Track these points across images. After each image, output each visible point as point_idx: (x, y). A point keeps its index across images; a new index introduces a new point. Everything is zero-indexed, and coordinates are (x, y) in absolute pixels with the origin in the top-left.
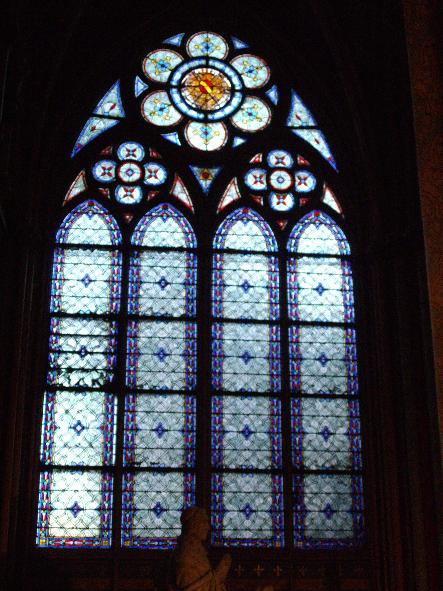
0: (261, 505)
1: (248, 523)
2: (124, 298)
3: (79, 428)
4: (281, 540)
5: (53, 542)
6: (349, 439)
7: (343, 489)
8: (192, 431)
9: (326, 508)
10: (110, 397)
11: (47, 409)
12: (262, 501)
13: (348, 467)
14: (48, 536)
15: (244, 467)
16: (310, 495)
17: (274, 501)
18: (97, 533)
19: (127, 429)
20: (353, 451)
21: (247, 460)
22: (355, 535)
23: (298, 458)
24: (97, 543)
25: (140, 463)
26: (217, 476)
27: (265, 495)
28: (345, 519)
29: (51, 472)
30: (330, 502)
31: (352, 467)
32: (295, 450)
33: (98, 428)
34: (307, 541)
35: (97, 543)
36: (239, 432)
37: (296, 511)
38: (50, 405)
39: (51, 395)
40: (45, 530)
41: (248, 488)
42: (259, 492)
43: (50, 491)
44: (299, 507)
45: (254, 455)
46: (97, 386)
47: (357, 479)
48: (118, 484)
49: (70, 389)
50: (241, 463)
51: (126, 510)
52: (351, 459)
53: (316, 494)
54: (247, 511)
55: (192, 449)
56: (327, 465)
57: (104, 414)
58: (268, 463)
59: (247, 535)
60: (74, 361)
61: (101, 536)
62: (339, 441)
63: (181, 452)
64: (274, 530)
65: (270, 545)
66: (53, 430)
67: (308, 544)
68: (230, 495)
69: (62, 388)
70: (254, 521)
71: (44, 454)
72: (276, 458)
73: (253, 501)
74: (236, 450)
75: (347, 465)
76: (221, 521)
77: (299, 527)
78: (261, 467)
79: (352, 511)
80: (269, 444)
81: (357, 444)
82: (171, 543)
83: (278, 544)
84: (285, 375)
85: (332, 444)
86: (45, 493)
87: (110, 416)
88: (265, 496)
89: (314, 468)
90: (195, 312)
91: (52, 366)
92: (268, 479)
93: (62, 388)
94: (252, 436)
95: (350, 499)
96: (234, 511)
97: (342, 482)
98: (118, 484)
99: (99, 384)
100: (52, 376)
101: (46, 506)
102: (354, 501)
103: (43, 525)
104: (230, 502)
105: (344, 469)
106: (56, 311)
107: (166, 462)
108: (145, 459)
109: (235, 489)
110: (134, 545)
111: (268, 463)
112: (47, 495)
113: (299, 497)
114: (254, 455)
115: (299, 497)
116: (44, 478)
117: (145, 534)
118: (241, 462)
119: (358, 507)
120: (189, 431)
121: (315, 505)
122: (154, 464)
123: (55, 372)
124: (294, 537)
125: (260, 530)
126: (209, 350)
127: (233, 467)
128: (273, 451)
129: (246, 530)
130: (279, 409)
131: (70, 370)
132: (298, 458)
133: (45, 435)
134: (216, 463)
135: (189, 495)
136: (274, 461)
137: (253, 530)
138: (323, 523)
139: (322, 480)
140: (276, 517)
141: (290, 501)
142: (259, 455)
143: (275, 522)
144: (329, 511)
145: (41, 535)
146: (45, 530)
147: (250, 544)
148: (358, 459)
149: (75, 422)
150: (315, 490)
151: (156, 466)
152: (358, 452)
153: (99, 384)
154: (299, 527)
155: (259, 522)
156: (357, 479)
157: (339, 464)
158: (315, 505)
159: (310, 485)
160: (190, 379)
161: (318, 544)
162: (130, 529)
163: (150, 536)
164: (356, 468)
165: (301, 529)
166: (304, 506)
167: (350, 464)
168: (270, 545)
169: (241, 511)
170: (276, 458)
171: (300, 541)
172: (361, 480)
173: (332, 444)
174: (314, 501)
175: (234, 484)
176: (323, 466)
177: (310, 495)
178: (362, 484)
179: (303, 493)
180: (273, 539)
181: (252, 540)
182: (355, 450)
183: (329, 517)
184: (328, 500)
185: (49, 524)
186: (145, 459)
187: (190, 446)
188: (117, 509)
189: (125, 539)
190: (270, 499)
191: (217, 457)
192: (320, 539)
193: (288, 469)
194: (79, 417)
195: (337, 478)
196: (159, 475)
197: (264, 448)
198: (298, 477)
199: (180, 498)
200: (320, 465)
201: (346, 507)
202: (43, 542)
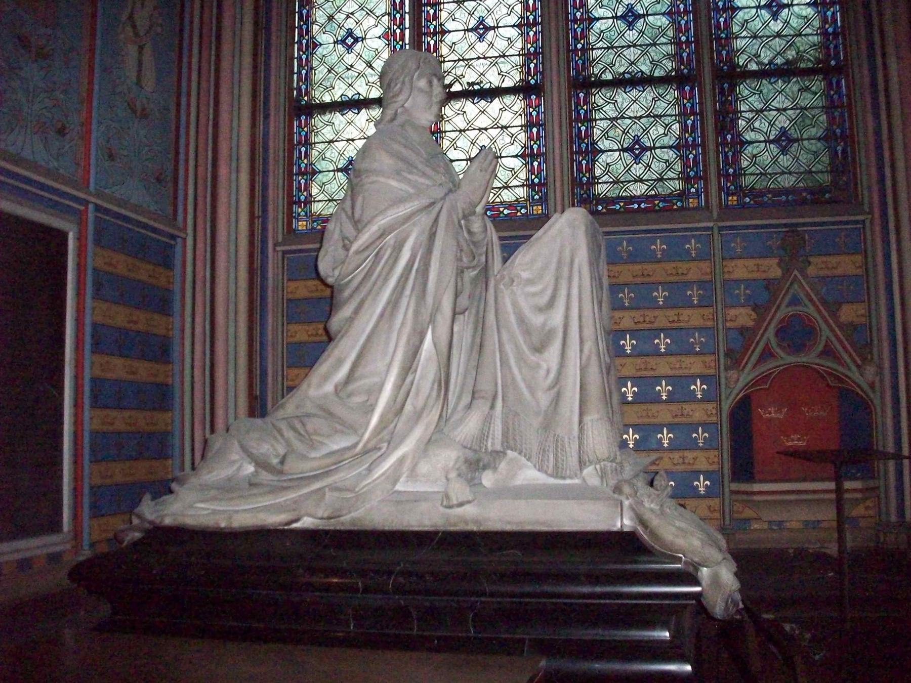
0: (659, 137)
1: (638, 170)
3: (350, 41)
4: (698, 194)
5: (318, 225)
6: (819, 12)
7: (806, 100)
8: (535, 24)
11: (301, 18)
12: (661, 130)
13: (818, 61)
14: (309, 215)
15: (627, 76)
16: (749, 115)
17: (684, 128)
19: (427, 34)
20: (825, 34)
21: (632, 63)
23: (724, 53)
24: (523, 211)
27: (668, 120)
28: (815, 153)
29: (310, 115)
31: (826, 61)
33: (379, 37)
36: (615, 17)
40: (305, 206)
41: (636, 110)
42: (655, 116)
43: (311, 144)
44: (729, 137)
45: (644, 53)
47: (834, 81)
50: (622, 70)
52: (824, 46)
53: (759, 112)
54: (636, 149)
55: (536, 54)
56: (779, 61)
57: (389, 14)
58: (669, 65)
59: (638, 189)
62: (799, 16)
63: (517, 60)
64: (686, 179)
66: (310, 50)
67: (747, 200)
68: (604, 124)
70: (648, 166)
71: (299, 89)
72: (685, 55)
73: (646, 131)
74: (612, 47)
75: (816, 58)
76: (591, 170)
77: (731, 171)
78: (658, 73)
80: (670, 33)
81: (834, 20)
82: (506, 212)
83: (692, 203)
85: (787, 23)
86: (303, 149)
87: (398, 16)
88: (666, 122)
89: (753, 67)
92: (672, 94)
94: (640, 23)
95: (824, 118)
96: (750, 7)
97: (807, 89)
101: (306, 168)
102: (831, 120)
103: (303, 198)
104: (605, 135)
105: (810, 65)
107: (493, 79)
108: (457, 79)
109: (613, 114)
111: (669, 65)
112: (306, 152)
114: (644, 53)
116: (300, 126)
118: (621, 67)
120: (529, 25)
121: (759, 131)
122: (473, 84)
125: (661, 179)
127: (608, 76)
128: (677, 43)
129: (636, 181)
132: (724, 53)
133: (300, 59)
134: (578, 73)
135: (535, 130)
137: (647, 181)
138: (775, 160)
139: (771, 87)
140: (687, 157)
141: (712, 128)
142: (654, 53)
143: (685, 165)
144: (784, 141)
145: (299, 215)
146: (305, 206)
148: (836, 47)
149: (343, 33)
150: (759, 106)
151: (476, 87)
152: (835, 34)
154: (731, 171)
155: (657, 166)
157: (800, 57)
158: (759, 131)
159: (749, 98)
164: (532, 82)
166: (740, 135)
168: (679, 204)
169: (624, 150)
170: (685, 55)
171: (733, 194)
173: (787, 23)
174: (757, 124)
175: (612, 106)
176: (771, 62)
177: (749, 115)
179: (737, 112)
180: (683, 195)
181: (646, 198)
182: (830, 30)
183: (784, 151)
184: (783, 122)
185: (311, 195)
186: (457, 79)
190: (676, 127)
192: (769, 191)
194: (350, 24)
195: (797, 81)
196: (483, 103)
197: (663, 40)
198: (726, 85)
199: (594, 38)
200: (766, 61)
202: (302, 225)
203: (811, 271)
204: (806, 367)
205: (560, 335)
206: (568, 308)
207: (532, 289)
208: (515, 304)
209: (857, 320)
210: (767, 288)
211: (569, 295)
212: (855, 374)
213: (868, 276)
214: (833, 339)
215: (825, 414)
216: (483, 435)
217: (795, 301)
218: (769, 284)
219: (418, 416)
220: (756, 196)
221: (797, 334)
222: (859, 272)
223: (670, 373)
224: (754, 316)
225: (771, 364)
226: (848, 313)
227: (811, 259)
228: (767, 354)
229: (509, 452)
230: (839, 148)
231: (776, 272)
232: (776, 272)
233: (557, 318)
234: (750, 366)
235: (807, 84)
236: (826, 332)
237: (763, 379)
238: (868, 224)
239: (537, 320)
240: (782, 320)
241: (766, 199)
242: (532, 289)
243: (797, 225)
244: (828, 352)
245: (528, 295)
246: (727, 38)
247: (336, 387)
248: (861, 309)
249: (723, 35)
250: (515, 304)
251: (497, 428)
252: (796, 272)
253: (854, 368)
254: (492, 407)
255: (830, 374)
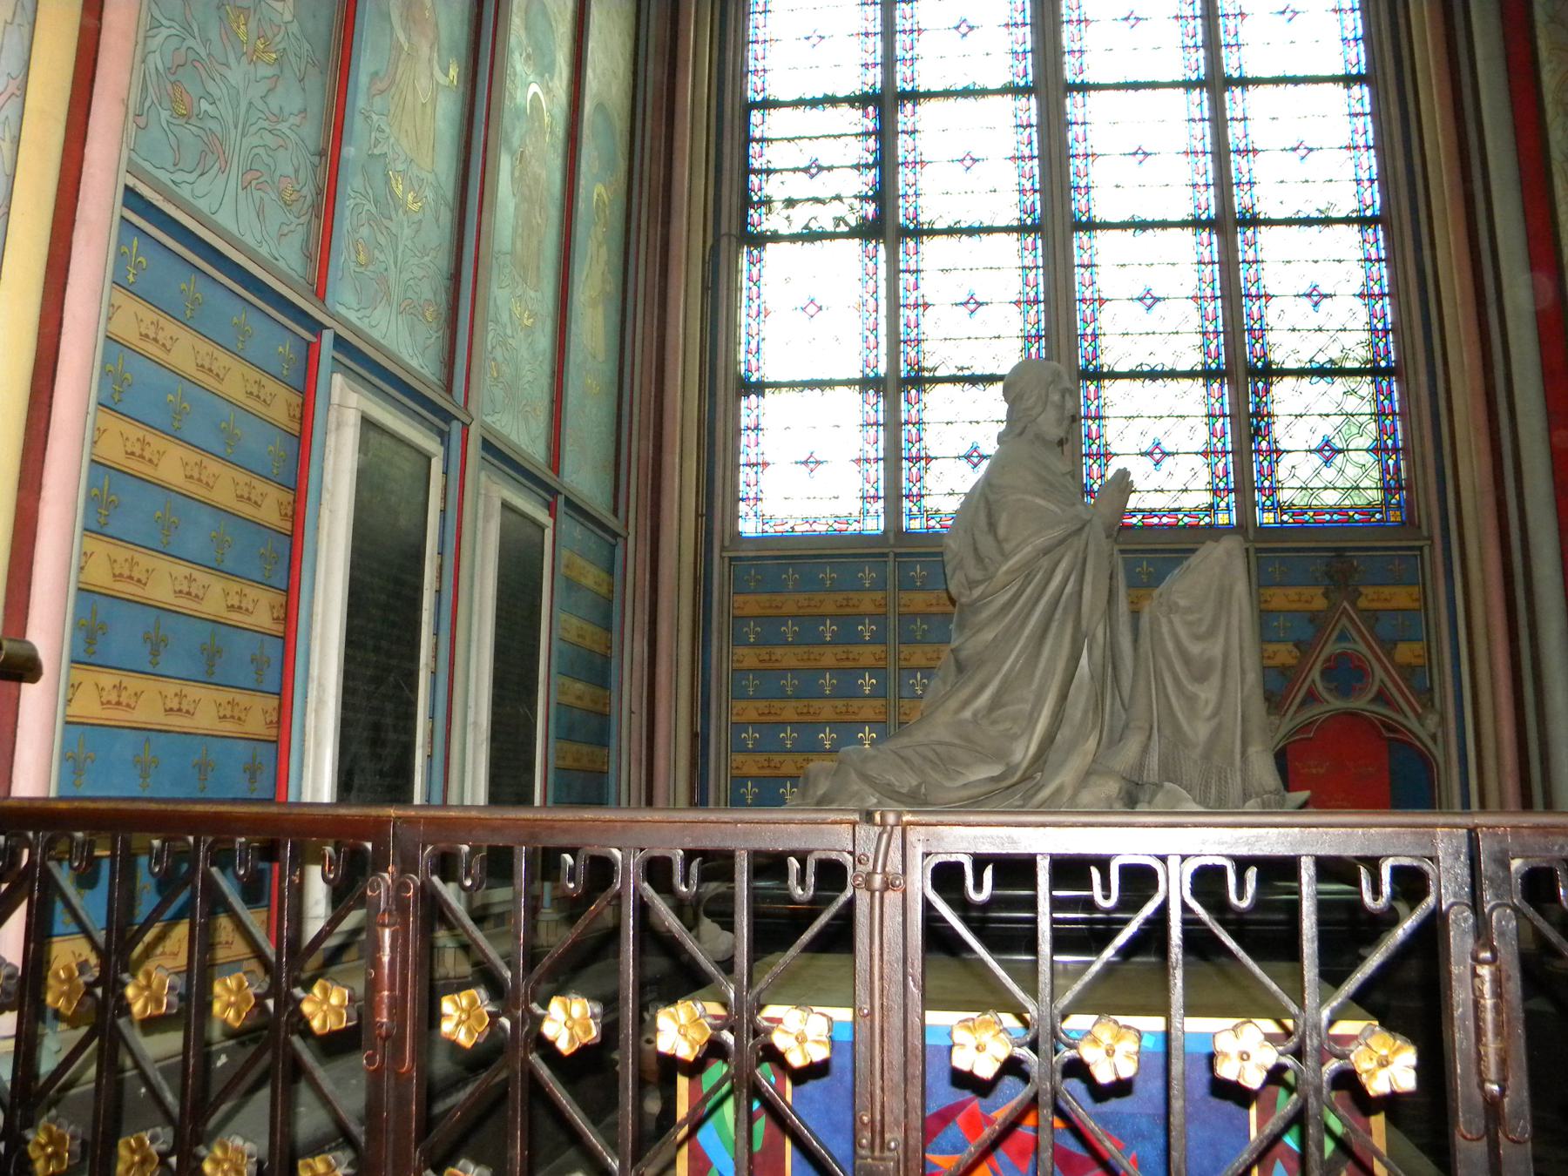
2: (889, 62)
9: (1329, 448)
10: (871, 246)
11: (750, 279)
18: (1206, 498)
20: (1374, 331)
22: (1385, 498)
24: (1378, 516)
25: (935, 369)
26: (1092, 388)
30: (1330, 432)
32: (1251, 330)
34: (1283, 512)
35: (1378, 516)
37: (1259, 451)
38: (755, 271)
39: (755, 253)
44: (1264, 445)
46: (843, 228)
48: (893, 410)
49: (793, 238)
51: (909, 459)
60: (799, 186)
61: (1386, 503)
65: (1207, 520)
67: (1285, 518)
69: (776, 237)
72: (1213, 347)
79: (1378, 449)
83: (1222, 519)
84: (1223, 184)
90: (1030, 78)
91: (755, 199)
93: (776, 237)
98: (893, 410)
99: (847, 224)
100: (756, 216)
105: (1357, 365)
106: (759, 99)
110: (1283, 522)
113: (1262, 424)
115: (1262, 424)
117: (1300, 500)
119: (1390, 442)
123: (763, 209)
124: (1255, 504)
126: (1064, 146)
130: (1212, 251)
131: (790, 203)
132: (1258, 346)
136: (1208, 354)
144: (1328, 451)
147: (1165, 520)
151: (967, 373)
153: (847, 224)
156: (1384, 384)
159: (1285, 396)
160: (1028, 203)
161: (1306, 517)
162: (1273, 490)
163: (1315, 502)
164: (1383, 364)
165: (1270, 488)
167: (1370, 356)
172: (1394, 387)
178: (1396, 396)
180: (1212, 509)
182: (1380, 326)
187: (1033, 332)
188: (893, 458)
189: (911, 517)
191: (1090, 349)
193: (1241, 371)
198: (1260, 385)
201: (1366, 441)
203: (1363, 603)
204: (1353, 715)
205: (1220, 666)
206: (1227, 639)
207: (1190, 618)
208: (1175, 635)
209: (1414, 661)
210: (1311, 621)
211: (1228, 624)
212: (1413, 724)
213: (1426, 610)
214: (1390, 685)
215: (1322, 771)
216: (1141, 766)
217: (1343, 637)
218: (1314, 617)
219: (1072, 746)
220: (1294, 514)
221: (1345, 673)
222: (1416, 605)
223: (796, 718)
224: (1296, 652)
225: (1314, 711)
226: (1406, 652)
227: (1361, 589)
228: (1312, 697)
229: (1167, 785)
230: (1391, 462)
231: (1320, 603)
232: (1320, 603)
233: (1216, 650)
234: (1293, 708)
235: (1353, 386)
236: (1379, 673)
237: (1305, 728)
238: (1426, 551)
239: (1195, 649)
240: (1328, 660)
241: (1306, 517)
242: (1190, 618)
243: (1345, 549)
244: (1382, 697)
245: (1190, 624)
246: (1261, 329)
247: (975, 715)
248: (1418, 647)
249: (1257, 326)
250: (1175, 635)
251: (1154, 761)
252: (1345, 604)
253: (1410, 714)
254: (1149, 737)
255: (1384, 724)
